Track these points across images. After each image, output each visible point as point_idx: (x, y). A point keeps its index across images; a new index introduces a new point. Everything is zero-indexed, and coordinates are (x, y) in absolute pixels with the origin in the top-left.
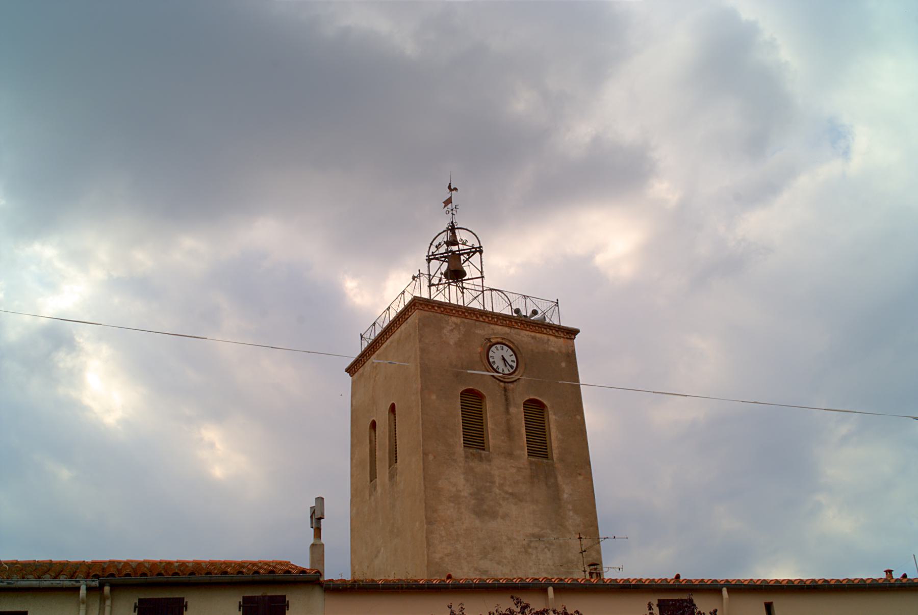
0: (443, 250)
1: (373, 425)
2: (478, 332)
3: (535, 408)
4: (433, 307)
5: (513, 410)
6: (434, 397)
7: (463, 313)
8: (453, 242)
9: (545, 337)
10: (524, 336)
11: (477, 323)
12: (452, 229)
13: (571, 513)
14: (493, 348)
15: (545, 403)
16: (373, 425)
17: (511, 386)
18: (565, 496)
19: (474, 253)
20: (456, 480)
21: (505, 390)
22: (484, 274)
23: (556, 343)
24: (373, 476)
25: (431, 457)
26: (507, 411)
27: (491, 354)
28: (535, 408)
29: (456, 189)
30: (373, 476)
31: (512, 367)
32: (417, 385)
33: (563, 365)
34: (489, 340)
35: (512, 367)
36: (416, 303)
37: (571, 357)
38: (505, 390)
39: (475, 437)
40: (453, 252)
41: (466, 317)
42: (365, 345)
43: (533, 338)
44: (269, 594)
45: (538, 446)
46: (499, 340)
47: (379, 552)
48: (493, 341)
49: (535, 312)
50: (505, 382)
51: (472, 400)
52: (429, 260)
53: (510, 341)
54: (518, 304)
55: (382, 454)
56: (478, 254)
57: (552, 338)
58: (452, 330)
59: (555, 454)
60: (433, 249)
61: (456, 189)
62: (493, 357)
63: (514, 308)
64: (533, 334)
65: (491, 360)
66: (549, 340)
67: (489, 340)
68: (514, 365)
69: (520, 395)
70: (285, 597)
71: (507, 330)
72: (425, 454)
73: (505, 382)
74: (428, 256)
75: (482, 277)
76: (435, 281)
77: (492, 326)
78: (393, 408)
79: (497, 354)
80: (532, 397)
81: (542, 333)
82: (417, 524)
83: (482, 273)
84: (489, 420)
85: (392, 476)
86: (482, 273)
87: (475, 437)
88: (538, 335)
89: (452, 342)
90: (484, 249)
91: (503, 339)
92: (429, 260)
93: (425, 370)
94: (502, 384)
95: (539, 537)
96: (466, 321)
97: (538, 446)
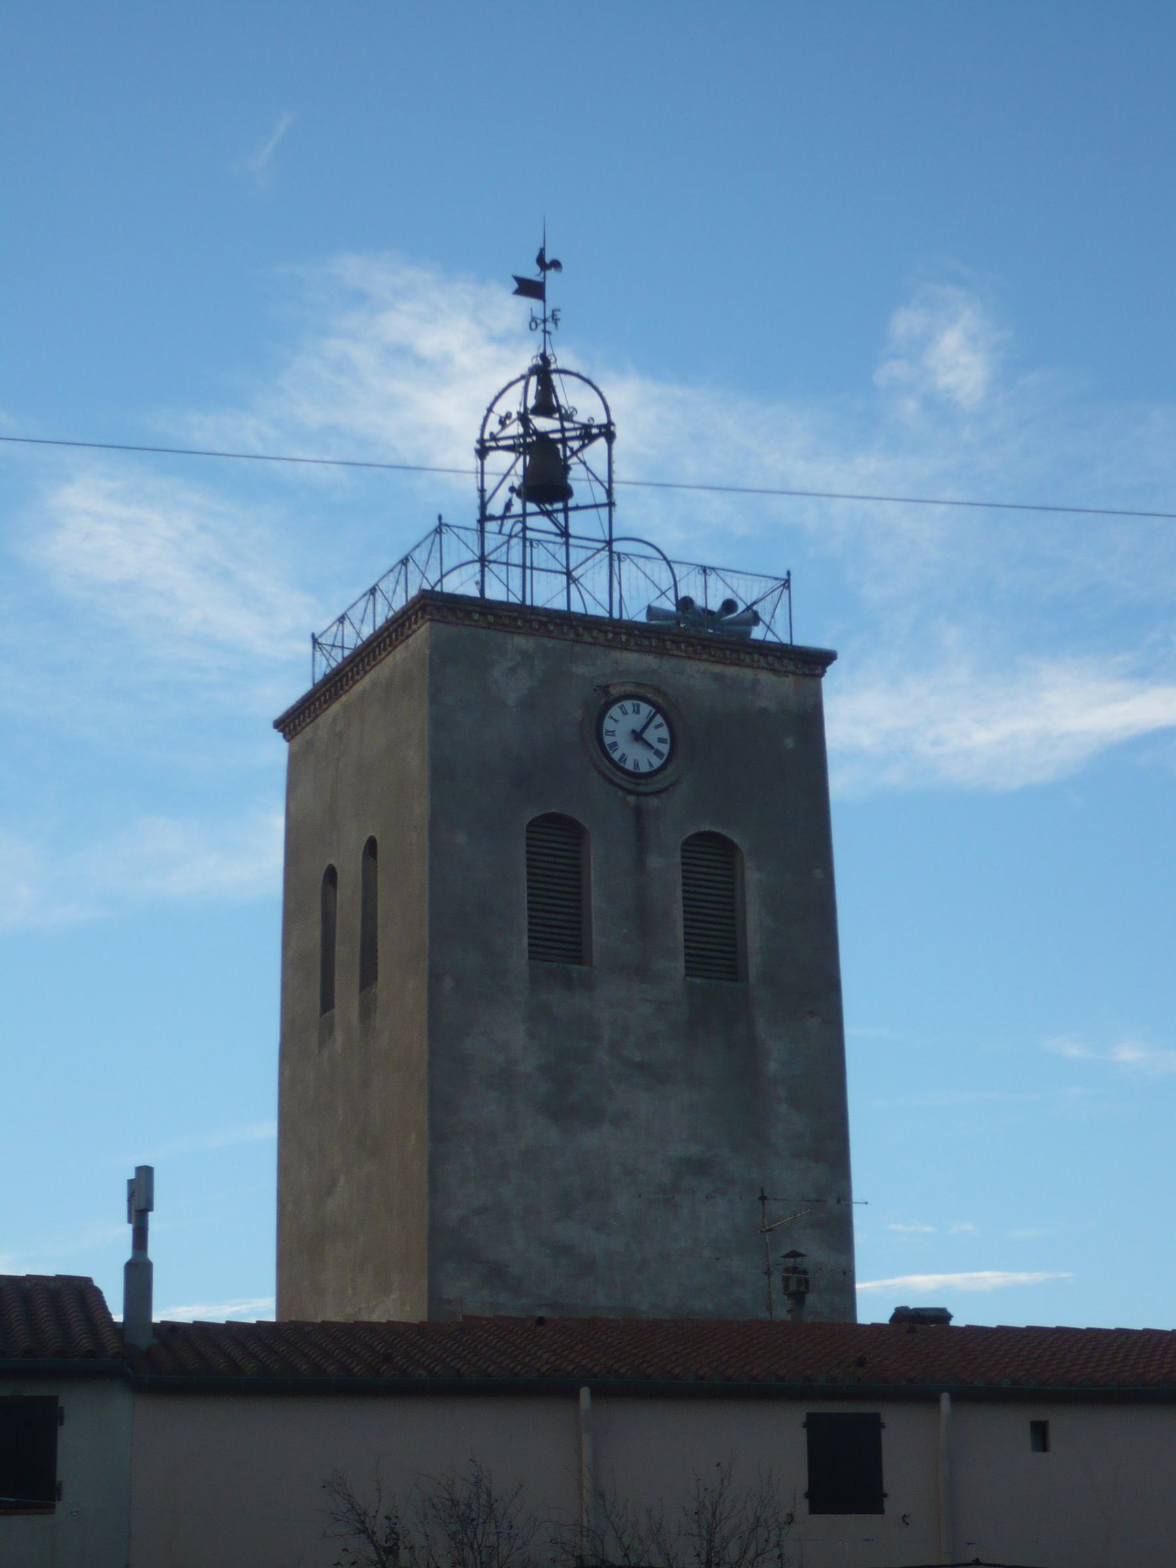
0: (515, 429)
1: (331, 875)
2: (580, 669)
3: (711, 856)
4: (469, 614)
5: (654, 862)
6: (461, 838)
7: (541, 623)
8: (546, 405)
9: (748, 674)
10: (695, 675)
11: (578, 648)
12: (543, 372)
13: (783, 1108)
14: (615, 711)
15: (736, 839)
16: (331, 875)
17: (654, 802)
18: (772, 1066)
19: (592, 438)
20: (508, 1037)
21: (638, 812)
22: (616, 497)
23: (773, 687)
24: (327, 1003)
25: (448, 983)
26: (640, 865)
27: (608, 724)
28: (711, 856)
29: (556, 264)
30: (327, 1003)
31: (658, 753)
32: (421, 809)
33: (790, 743)
34: (605, 689)
35: (658, 753)
36: (432, 605)
37: (810, 724)
38: (638, 812)
39: (559, 936)
40: (543, 436)
41: (550, 635)
42: (323, 668)
43: (718, 678)
44: (25, 1394)
45: (715, 949)
46: (630, 688)
47: (334, 1183)
48: (615, 691)
49: (729, 606)
50: (638, 794)
51: (557, 848)
52: (482, 452)
53: (657, 690)
54: (692, 588)
55: (347, 953)
56: (601, 442)
57: (765, 677)
58: (513, 670)
59: (754, 963)
60: (493, 426)
61: (556, 264)
62: (612, 733)
63: (681, 595)
64: (717, 669)
65: (608, 740)
66: (756, 682)
67: (605, 689)
68: (665, 749)
69: (676, 822)
70: (56, 1399)
71: (650, 661)
72: (435, 977)
73: (638, 794)
74: (482, 441)
75: (611, 504)
76: (495, 508)
77: (616, 654)
78: (371, 847)
79: (621, 722)
80: (705, 827)
81: (738, 663)
82: (413, 1136)
83: (609, 492)
84: (594, 889)
85: (367, 1011)
86: (609, 492)
87: (559, 936)
88: (731, 671)
89: (512, 699)
90: (619, 430)
91: (639, 685)
92: (482, 452)
93: (442, 773)
94: (631, 799)
95: (701, 1167)
96: (550, 643)
97: (715, 949)
